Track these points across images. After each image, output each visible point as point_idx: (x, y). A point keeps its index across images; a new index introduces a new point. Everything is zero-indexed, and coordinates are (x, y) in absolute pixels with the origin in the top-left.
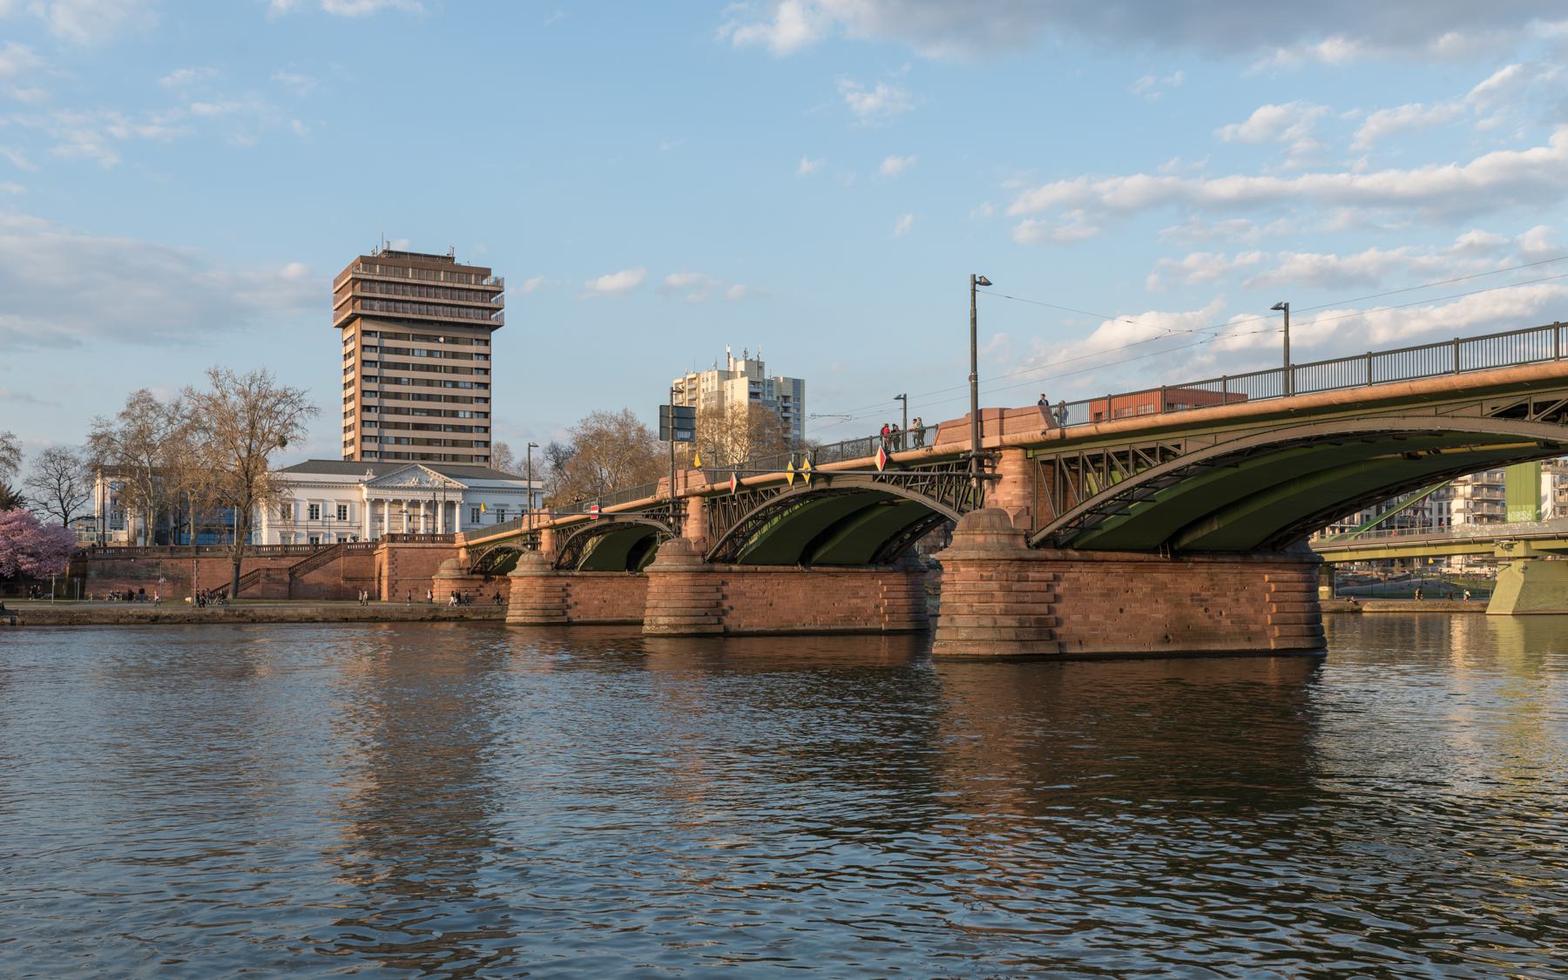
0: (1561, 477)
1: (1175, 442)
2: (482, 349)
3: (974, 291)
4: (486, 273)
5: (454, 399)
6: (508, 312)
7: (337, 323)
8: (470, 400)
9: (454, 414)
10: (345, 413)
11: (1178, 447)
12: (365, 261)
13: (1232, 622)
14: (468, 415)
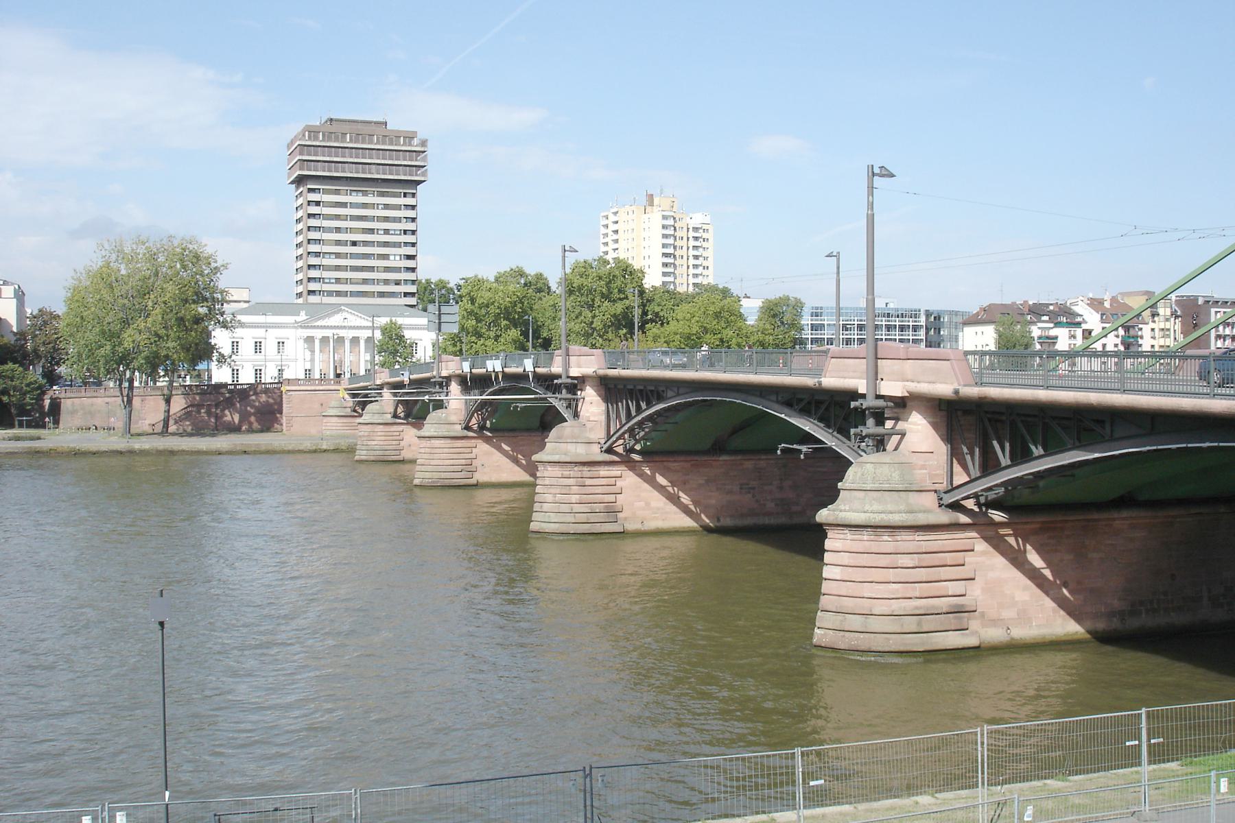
0: (631, 389)
2: (410, 201)
3: (871, 188)
4: (410, 137)
5: (386, 244)
7: (289, 182)
8: (397, 245)
9: (385, 257)
10: (297, 233)
12: (313, 132)
13: (776, 505)
14: (398, 258)
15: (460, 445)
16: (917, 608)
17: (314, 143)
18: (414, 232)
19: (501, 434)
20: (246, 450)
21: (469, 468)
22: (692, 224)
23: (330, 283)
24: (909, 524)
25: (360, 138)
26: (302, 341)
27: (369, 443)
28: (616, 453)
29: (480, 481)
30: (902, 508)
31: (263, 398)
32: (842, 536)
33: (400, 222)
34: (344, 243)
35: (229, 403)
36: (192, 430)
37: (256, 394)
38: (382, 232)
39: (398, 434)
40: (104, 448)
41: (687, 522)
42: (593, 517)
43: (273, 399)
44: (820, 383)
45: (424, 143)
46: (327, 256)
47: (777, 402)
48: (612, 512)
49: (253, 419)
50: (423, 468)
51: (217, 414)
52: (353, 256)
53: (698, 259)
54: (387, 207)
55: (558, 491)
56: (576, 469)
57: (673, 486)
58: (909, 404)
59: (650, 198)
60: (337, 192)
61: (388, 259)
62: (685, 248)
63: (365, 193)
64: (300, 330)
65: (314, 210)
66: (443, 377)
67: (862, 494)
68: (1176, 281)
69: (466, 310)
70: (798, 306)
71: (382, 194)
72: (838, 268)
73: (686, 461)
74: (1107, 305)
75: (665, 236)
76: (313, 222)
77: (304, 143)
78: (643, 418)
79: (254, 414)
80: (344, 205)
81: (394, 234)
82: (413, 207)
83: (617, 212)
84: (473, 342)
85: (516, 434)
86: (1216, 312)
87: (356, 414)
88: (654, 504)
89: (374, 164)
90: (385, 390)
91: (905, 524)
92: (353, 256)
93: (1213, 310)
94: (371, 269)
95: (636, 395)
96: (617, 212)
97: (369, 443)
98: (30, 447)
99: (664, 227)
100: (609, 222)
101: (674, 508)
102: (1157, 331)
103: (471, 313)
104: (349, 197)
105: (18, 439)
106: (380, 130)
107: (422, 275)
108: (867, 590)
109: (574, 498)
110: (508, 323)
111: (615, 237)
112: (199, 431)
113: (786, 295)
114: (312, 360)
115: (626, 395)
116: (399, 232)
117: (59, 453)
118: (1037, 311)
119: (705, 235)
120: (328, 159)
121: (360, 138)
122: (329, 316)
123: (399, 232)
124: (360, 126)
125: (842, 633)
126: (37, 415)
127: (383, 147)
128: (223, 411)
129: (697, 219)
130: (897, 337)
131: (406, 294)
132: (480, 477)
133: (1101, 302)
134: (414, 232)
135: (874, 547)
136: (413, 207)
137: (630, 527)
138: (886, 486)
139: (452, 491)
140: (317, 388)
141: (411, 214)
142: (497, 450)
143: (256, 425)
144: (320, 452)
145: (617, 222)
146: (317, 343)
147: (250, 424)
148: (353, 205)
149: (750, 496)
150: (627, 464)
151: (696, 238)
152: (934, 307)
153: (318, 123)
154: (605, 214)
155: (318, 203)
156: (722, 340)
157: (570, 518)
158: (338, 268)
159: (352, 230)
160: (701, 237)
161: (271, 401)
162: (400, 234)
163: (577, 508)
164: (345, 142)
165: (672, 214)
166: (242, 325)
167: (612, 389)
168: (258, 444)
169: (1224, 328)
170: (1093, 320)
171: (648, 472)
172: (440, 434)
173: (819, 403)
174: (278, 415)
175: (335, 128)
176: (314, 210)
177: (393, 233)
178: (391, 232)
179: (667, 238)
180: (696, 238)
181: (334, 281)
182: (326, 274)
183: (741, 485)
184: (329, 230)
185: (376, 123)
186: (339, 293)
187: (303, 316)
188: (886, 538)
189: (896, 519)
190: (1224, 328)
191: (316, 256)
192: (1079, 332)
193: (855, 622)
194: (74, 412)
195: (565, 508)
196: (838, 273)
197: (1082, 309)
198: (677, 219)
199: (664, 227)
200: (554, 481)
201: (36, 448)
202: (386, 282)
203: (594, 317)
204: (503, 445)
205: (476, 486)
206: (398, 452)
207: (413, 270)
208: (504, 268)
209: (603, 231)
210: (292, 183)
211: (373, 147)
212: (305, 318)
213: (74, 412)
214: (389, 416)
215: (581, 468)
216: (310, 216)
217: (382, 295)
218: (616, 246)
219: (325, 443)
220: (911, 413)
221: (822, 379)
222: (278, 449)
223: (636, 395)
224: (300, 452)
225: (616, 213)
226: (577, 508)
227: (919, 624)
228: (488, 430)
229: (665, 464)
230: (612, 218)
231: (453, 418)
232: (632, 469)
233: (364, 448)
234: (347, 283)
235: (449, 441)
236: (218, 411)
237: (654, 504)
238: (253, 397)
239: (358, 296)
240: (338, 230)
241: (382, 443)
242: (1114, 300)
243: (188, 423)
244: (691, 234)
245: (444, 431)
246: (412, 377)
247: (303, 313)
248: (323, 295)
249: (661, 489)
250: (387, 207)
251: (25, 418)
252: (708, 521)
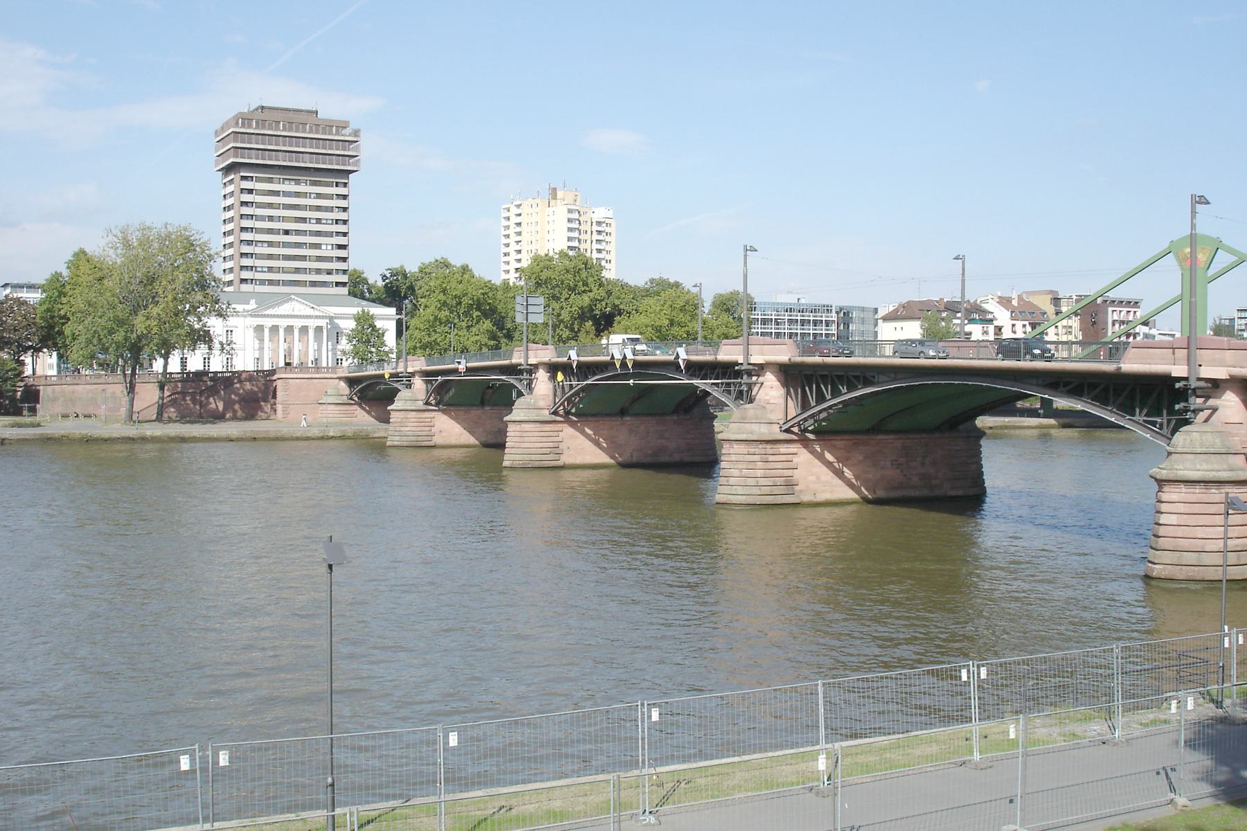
1: (872, 374)
3: (746, 256)
4: (343, 126)
5: (318, 234)
6: (363, 167)
11: (874, 377)
12: (245, 119)
13: (920, 479)
14: (330, 247)
15: (547, 429)
16: (1237, 546)
17: (248, 131)
18: (345, 222)
19: (584, 419)
20: (256, 437)
21: (557, 451)
22: (596, 218)
23: (262, 272)
24: (1233, 479)
25: (294, 127)
26: (252, 330)
27: (402, 429)
28: (793, 433)
29: (567, 463)
30: (1225, 467)
31: (248, 386)
32: (1178, 490)
33: (332, 212)
34: (277, 232)
35: (213, 391)
36: (177, 417)
37: (240, 382)
38: (314, 221)
39: (429, 420)
40: (115, 435)
41: (851, 495)
42: (776, 490)
43: (257, 387)
44: (1120, 368)
45: (356, 133)
46: (260, 244)
47: (1038, 385)
48: (790, 484)
49: (237, 407)
50: (513, 451)
51: (202, 401)
52: (286, 245)
53: (600, 253)
54: (319, 196)
55: (745, 466)
56: (760, 446)
57: (838, 462)
58: (1222, 385)
59: (554, 193)
60: (270, 180)
61: (320, 248)
62: (589, 242)
63: (298, 182)
64: (249, 319)
65: (246, 197)
66: (531, 365)
67: (1192, 456)
68: (1109, 283)
69: (439, 301)
71: (314, 183)
72: (963, 269)
73: (848, 440)
74: (1015, 303)
75: (570, 230)
76: (246, 210)
77: (238, 130)
79: (239, 402)
80: (276, 193)
81: (327, 224)
82: (345, 197)
83: (521, 205)
84: (447, 332)
85: (597, 419)
86: (1113, 311)
87: (353, 402)
88: (823, 478)
89: (307, 153)
90: (417, 377)
91: (1231, 479)
92: (286, 245)
93: (1110, 309)
94: (303, 258)
95: (817, 380)
96: (521, 205)
97: (402, 429)
98: (42, 434)
99: (570, 220)
100: (512, 214)
101: (840, 482)
102: (1060, 328)
103: (445, 304)
104: (281, 185)
105: (20, 426)
106: (311, 120)
107: (352, 265)
108: (1200, 532)
109: (759, 473)
110: (480, 314)
111: (518, 229)
112: (185, 418)
113: (736, 289)
114: (261, 349)
115: (802, 382)
116: (330, 222)
117: (71, 440)
118: (952, 308)
119: (608, 230)
120: (262, 147)
121: (294, 127)
122: (279, 304)
123: (330, 222)
124: (291, 114)
125: (1179, 567)
126: (7, 402)
127: (316, 136)
128: (207, 398)
129: (600, 213)
130: (760, 331)
131: (338, 284)
132: (566, 459)
133: (1009, 300)
134: (345, 222)
135: (1205, 498)
136: (345, 197)
137: (806, 498)
138: (1212, 450)
139: (536, 473)
140: (314, 376)
141: (343, 203)
142: (581, 433)
143: (240, 413)
144: (328, 439)
145: (520, 215)
146: (267, 332)
147: (235, 412)
148: (287, 194)
149: (898, 471)
150: (803, 443)
151: (599, 232)
152: (845, 302)
153: (246, 111)
154: (507, 206)
155: (250, 191)
156: (688, 333)
157: (756, 491)
158: (270, 257)
159: (285, 219)
160: (604, 231)
161: (255, 389)
162: (332, 224)
163: (763, 481)
164: (279, 130)
165: (577, 208)
166: (236, 313)
167: (792, 375)
168: (268, 431)
169: (1120, 326)
170: (1002, 317)
171: (819, 450)
172: (531, 418)
173: (1093, 386)
174: (262, 403)
175: (266, 115)
176: (246, 197)
177: (325, 222)
178: (323, 222)
179: (572, 231)
180: (599, 232)
181: (266, 270)
182: (258, 263)
183: (892, 461)
184: (261, 218)
185: (308, 112)
186: (271, 282)
187: (252, 305)
188: (1213, 491)
189: (1225, 475)
190: (1120, 326)
191: (248, 244)
192: (991, 329)
193: (1190, 558)
194: (55, 399)
195: (751, 482)
196: (963, 274)
197: (992, 306)
198: (582, 213)
199: (570, 220)
200: (740, 458)
201: (47, 434)
202: (318, 271)
203: (562, 308)
204: (586, 429)
205: (563, 467)
206: (429, 438)
207: (344, 259)
208: (429, 259)
209: (505, 223)
210: (222, 169)
211: (306, 135)
212: (255, 306)
213: (55, 399)
214: (421, 403)
215: (765, 446)
216: (244, 204)
217: (314, 284)
218: (519, 238)
219: (332, 430)
220: (1224, 392)
221: (1122, 365)
222: (287, 436)
223: (817, 380)
224: (308, 439)
225: (519, 206)
226: (763, 481)
227: (1238, 558)
228: (573, 414)
229: (833, 442)
230: (514, 210)
231: (542, 404)
232: (805, 447)
233: (396, 433)
234: (279, 272)
235: (538, 425)
236: (203, 399)
237: (823, 478)
238: (238, 385)
239: (290, 285)
240: (271, 218)
241: (414, 429)
242: (1020, 298)
243: (172, 410)
244: (595, 228)
245: (533, 416)
246: (469, 365)
247: (253, 302)
248: (256, 284)
249: (829, 465)
250: (319, 196)
251: (26, 405)
252: (867, 493)
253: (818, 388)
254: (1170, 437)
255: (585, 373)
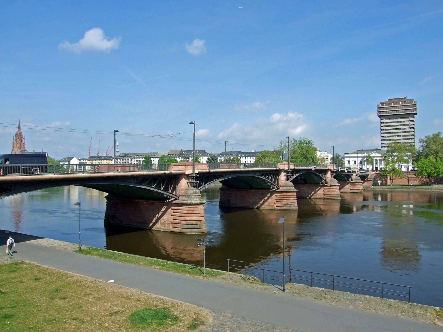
4: (411, 101)
38: (403, 129)
45: (415, 102)
48: (229, 201)
70: (340, 156)
78: (165, 173)
80: (391, 122)
148: (395, 122)
164: (400, 104)
253: (272, 177)
254: (342, 195)
255: (297, 172)
